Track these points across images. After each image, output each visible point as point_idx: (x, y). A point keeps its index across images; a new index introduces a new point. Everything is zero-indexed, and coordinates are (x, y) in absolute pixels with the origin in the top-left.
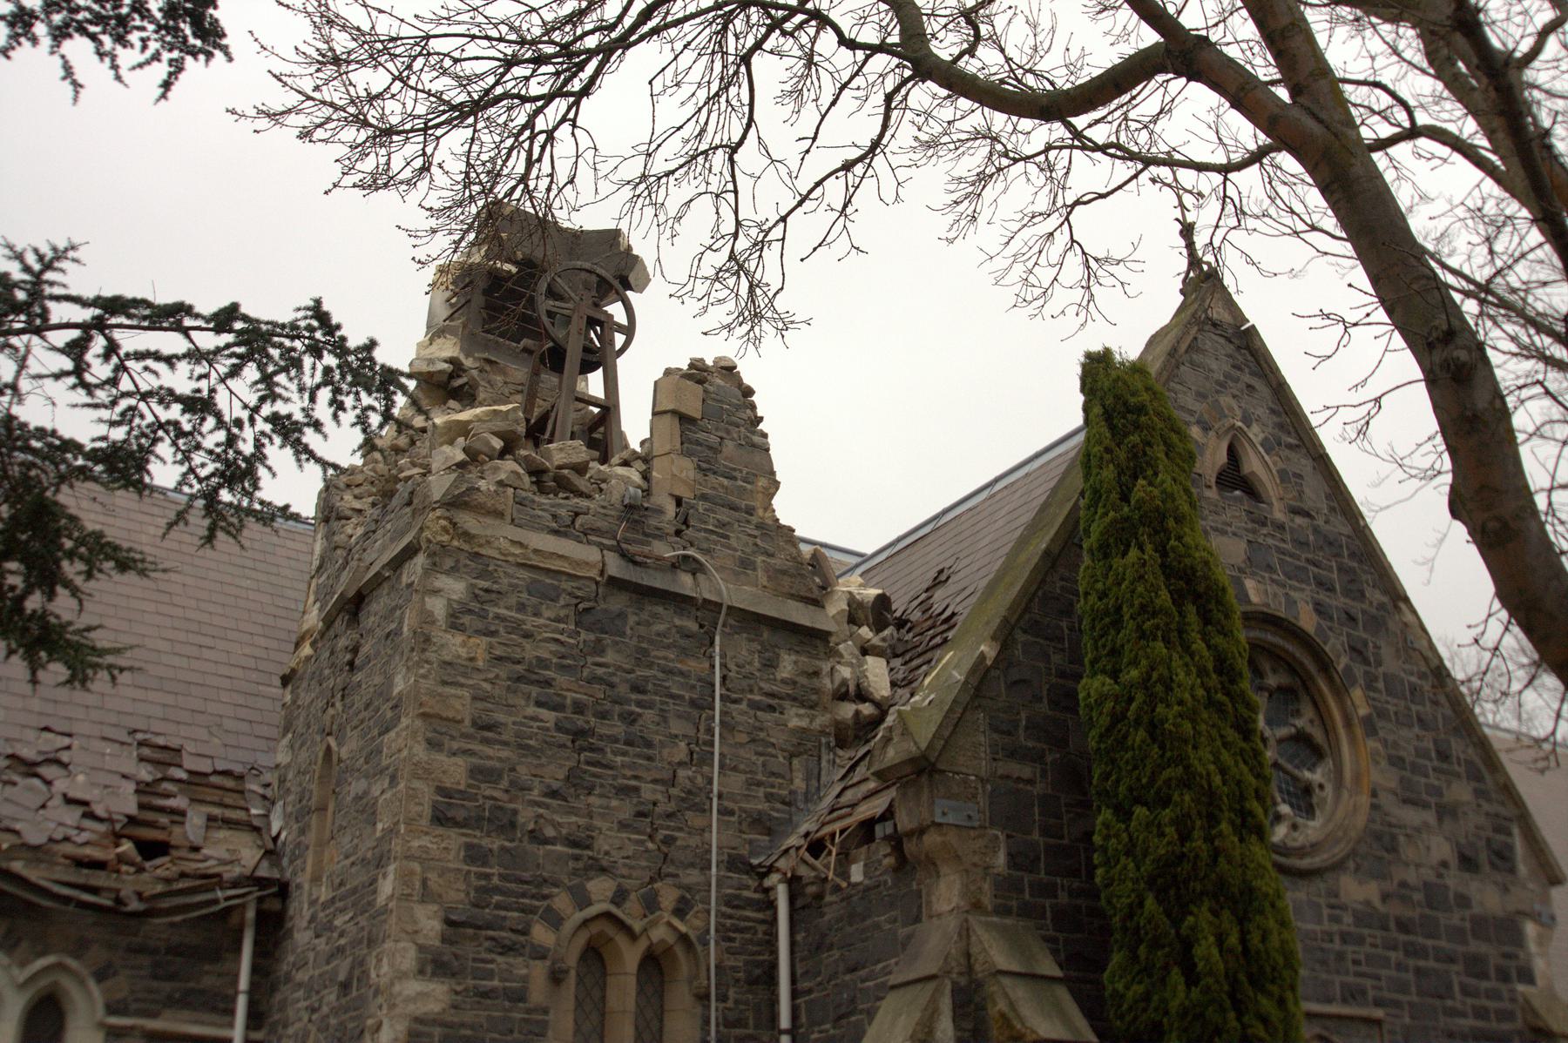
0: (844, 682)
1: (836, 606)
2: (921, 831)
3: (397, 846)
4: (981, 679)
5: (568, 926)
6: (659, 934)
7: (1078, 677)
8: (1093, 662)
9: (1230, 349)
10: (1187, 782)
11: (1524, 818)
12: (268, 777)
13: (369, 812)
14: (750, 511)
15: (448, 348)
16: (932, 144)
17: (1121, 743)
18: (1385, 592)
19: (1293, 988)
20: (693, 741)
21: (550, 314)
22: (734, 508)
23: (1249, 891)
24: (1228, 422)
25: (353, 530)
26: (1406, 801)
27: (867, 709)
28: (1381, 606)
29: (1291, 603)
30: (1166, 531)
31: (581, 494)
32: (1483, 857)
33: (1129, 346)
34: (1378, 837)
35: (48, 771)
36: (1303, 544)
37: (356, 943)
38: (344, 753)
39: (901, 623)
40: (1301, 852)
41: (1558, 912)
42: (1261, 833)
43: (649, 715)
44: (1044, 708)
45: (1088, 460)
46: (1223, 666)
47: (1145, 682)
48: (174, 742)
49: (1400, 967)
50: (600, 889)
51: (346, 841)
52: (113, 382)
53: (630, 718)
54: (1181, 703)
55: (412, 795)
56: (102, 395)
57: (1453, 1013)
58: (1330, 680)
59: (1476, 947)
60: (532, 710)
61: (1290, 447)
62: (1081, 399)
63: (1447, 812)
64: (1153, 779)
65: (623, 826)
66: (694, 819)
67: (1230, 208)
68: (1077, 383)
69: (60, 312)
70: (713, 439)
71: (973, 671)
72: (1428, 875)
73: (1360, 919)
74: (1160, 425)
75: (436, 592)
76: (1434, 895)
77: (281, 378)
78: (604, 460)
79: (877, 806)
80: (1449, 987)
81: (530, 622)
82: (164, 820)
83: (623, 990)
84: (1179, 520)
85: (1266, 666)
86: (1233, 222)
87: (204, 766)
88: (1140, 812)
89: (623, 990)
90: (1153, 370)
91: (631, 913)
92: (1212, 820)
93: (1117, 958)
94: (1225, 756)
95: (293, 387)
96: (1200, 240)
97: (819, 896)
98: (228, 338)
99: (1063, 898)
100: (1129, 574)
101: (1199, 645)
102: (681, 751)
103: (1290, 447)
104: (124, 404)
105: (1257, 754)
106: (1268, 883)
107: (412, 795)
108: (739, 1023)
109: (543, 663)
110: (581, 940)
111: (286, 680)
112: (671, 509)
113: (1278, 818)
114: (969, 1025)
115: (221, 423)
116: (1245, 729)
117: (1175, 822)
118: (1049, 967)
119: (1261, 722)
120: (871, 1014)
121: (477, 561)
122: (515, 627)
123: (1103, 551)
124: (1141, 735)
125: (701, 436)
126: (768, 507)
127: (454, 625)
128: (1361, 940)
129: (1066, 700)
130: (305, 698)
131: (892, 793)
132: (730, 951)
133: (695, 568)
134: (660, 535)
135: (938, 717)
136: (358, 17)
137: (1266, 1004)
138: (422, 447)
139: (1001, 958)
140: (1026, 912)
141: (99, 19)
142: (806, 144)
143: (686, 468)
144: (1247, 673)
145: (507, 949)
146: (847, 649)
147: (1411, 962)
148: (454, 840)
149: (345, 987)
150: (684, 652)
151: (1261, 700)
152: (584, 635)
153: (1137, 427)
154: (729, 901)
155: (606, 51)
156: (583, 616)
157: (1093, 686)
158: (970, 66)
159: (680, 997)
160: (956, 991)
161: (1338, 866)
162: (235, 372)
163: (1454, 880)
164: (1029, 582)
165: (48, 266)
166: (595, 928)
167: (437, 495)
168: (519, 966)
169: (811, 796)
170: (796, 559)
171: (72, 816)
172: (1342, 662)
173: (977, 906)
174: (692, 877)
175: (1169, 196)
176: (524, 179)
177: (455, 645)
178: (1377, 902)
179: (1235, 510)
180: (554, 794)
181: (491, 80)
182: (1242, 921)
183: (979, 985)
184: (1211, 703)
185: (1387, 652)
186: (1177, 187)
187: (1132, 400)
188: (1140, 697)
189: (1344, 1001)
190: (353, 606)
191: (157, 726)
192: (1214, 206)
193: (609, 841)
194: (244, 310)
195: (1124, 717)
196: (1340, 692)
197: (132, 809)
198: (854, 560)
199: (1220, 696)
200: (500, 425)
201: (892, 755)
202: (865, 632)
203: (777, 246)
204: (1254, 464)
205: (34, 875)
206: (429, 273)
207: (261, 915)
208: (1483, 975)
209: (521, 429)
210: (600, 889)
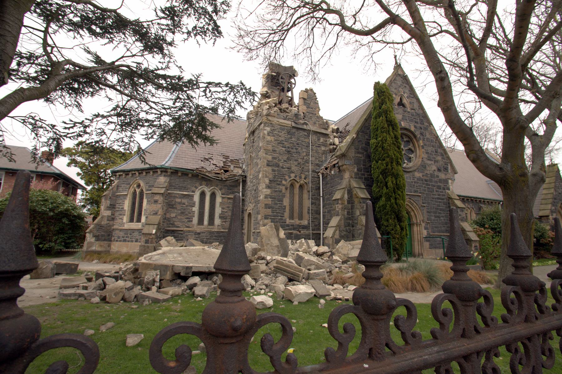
1: (330, 130)
2: (343, 165)
4: (353, 141)
6: (302, 182)
13: (257, 165)
14: (315, 114)
15: (266, 89)
21: (282, 82)
22: (313, 114)
31: (288, 113)
33: (383, 81)
43: (300, 148)
45: (374, 102)
46: (396, 137)
50: (293, 175)
55: (263, 161)
65: (296, 166)
69: (201, 85)
70: (309, 102)
76: (432, 175)
79: (336, 162)
81: (280, 134)
83: (297, 190)
89: (297, 190)
91: (297, 179)
109: (282, 140)
110: (290, 183)
112: (302, 114)
114: (350, 195)
116: (399, 148)
122: (278, 135)
123: (376, 118)
125: (307, 102)
133: (306, 124)
140: (360, 178)
145: (279, 185)
146: (332, 137)
148: (270, 168)
150: (305, 138)
154: (312, 177)
159: (305, 191)
160: (348, 190)
161: (415, 171)
167: (265, 114)
168: (281, 187)
170: (323, 122)
171: (214, 167)
173: (352, 177)
174: (307, 173)
177: (269, 138)
179: (401, 109)
180: (285, 161)
190: (253, 133)
193: (294, 168)
196: (418, 141)
198: (333, 122)
200: (274, 102)
201: (338, 153)
204: (405, 101)
209: (278, 102)
210: (293, 175)
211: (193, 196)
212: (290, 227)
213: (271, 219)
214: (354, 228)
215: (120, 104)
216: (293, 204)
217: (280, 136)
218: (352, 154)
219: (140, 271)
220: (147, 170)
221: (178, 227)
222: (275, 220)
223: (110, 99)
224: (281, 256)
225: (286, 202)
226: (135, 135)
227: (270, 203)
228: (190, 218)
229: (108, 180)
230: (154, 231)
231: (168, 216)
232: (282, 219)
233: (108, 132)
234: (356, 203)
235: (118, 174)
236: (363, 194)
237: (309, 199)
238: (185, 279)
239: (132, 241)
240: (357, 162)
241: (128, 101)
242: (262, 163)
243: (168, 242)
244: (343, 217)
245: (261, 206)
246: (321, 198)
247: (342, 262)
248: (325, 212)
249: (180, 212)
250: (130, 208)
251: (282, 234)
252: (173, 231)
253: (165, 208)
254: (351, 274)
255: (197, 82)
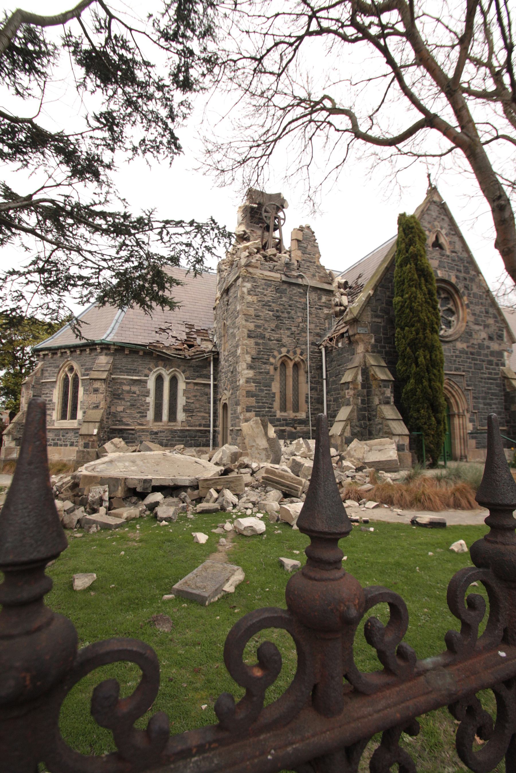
0: (337, 302)
1: (335, 284)
2: (354, 335)
3: (240, 343)
4: (369, 299)
5: (277, 358)
6: (297, 359)
7: (393, 297)
8: (397, 293)
9: (438, 209)
10: (419, 321)
11: (507, 327)
12: (212, 330)
13: (234, 336)
14: (314, 263)
15: (243, 228)
16: (359, 159)
17: (403, 313)
18: (475, 271)
19: (442, 368)
20: (302, 317)
21: (266, 217)
23: (433, 346)
24: (436, 229)
25: (225, 274)
26: (476, 324)
27: (342, 308)
28: (474, 275)
29: (449, 276)
30: (417, 259)
31: (275, 261)
32: (495, 337)
33: (410, 211)
34: (467, 333)
35: (168, 331)
36: (454, 260)
37: (234, 363)
38: (228, 323)
39: (350, 288)
40: (447, 337)
41: (514, 350)
42: (437, 332)
43: (293, 312)
44: (384, 305)
45: (398, 243)
46: (430, 293)
47: (410, 298)
48: (192, 324)
49: (470, 363)
50: (284, 350)
51: (230, 342)
52: (169, 241)
53: (289, 313)
54: (418, 302)
55: (243, 332)
56: (168, 244)
57: (483, 373)
58: (458, 295)
59: (490, 358)
60: (267, 312)
61: (453, 235)
62: (397, 226)
63: (486, 326)
64: (410, 320)
65: (288, 336)
66: (304, 335)
67: (441, 167)
68: (396, 222)
69: (155, 225)
70: (305, 245)
71: (367, 297)
72: (480, 341)
73: (461, 352)
74: (417, 231)
75: (244, 287)
76: (481, 346)
77: (205, 237)
78: (280, 253)
79: (345, 330)
80: (483, 368)
81: (266, 292)
82: (192, 340)
84: (421, 256)
85: (441, 292)
86: (442, 171)
87: (199, 328)
88: (407, 328)
90: (417, 217)
91: (291, 355)
92: (425, 330)
93: (400, 362)
94: (429, 315)
95: (209, 238)
96: (432, 178)
97: (332, 350)
98: (193, 228)
99: (387, 349)
100: (407, 271)
101: (424, 288)
102: (300, 320)
103: (453, 235)
104: (173, 246)
105: (437, 314)
106: (438, 344)
107: (243, 332)
108: (315, 377)
109: (269, 301)
110: (280, 361)
111: (214, 309)
112: (296, 263)
113: (442, 329)
114: (365, 377)
115: (194, 249)
116: (435, 308)
117: (415, 330)
118: (384, 364)
119: (439, 306)
120: (343, 375)
121: (252, 278)
122: (262, 293)
123: (401, 266)
124: (408, 310)
125: (302, 245)
126: (318, 261)
127: (249, 294)
128: (460, 357)
129: (390, 303)
130: (218, 312)
131: (348, 327)
132: (313, 363)
133: (302, 277)
134: (294, 270)
135: (359, 309)
136: (213, 139)
137: (435, 371)
138: (239, 253)
139: (373, 362)
140: (379, 352)
141: (152, 147)
142: (326, 162)
143: (299, 253)
144: (436, 294)
145: (265, 363)
146: (338, 294)
147: (473, 362)
148: (252, 341)
149: (232, 372)
150: (300, 297)
151: (439, 301)
152: (278, 295)
153: (412, 233)
154: (312, 352)
155: (275, 141)
156: (277, 290)
157: (397, 299)
158: (370, 133)
159: (302, 372)
160: (362, 369)
161: (456, 340)
162: (196, 236)
163: (486, 343)
164: (381, 275)
165: (151, 214)
166: (283, 359)
167: (243, 264)
169: (329, 328)
170: (326, 274)
171: (174, 340)
172: (462, 290)
173: (367, 351)
174: (303, 347)
175: (425, 166)
176: (257, 180)
177: (249, 298)
178: (465, 348)
180: (273, 330)
181: (247, 153)
182: (431, 352)
183: (367, 368)
184: (426, 302)
185: (474, 287)
186: (427, 163)
187: (411, 225)
188: (408, 301)
189: (455, 371)
190: (227, 291)
191: (189, 320)
192: (437, 166)
193: (286, 340)
194: (195, 221)
195: (404, 306)
196: (460, 298)
197: (186, 338)
198: (339, 273)
199: (429, 300)
200: (256, 246)
201: (348, 318)
202: (342, 290)
203: (319, 192)
204: (443, 240)
205: (168, 352)
206: (237, 209)
207: (214, 358)
208: (492, 365)
209: (261, 247)
210: (284, 350)
211: (146, 382)
212: (282, 422)
213: (254, 411)
214: (371, 422)
215: (42, 256)
216: (285, 389)
217: (265, 295)
218: (368, 318)
219: (81, 486)
220: (82, 348)
221: (128, 425)
222: (261, 413)
223: (27, 249)
224: (271, 463)
225: (276, 387)
226: (63, 298)
227: (253, 389)
228: (143, 413)
229: (28, 362)
230: (95, 432)
231: (113, 410)
232: (270, 412)
233: (28, 296)
234: (374, 387)
235: (41, 353)
236: (384, 375)
237: (307, 382)
238: (142, 496)
239: (66, 445)
240: (375, 330)
241: (53, 251)
242: (241, 334)
243: (115, 445)
244: (355, 407)
245: (241, 394)
246: (325, 381)
247: (356, 469)
248: (330, 401)
249: (129, 404)
250: (61, 400)
251: (272, 432)
252: (121, 430)
253: (109, 400)
254: (368, 486)
255: (149, 221)
